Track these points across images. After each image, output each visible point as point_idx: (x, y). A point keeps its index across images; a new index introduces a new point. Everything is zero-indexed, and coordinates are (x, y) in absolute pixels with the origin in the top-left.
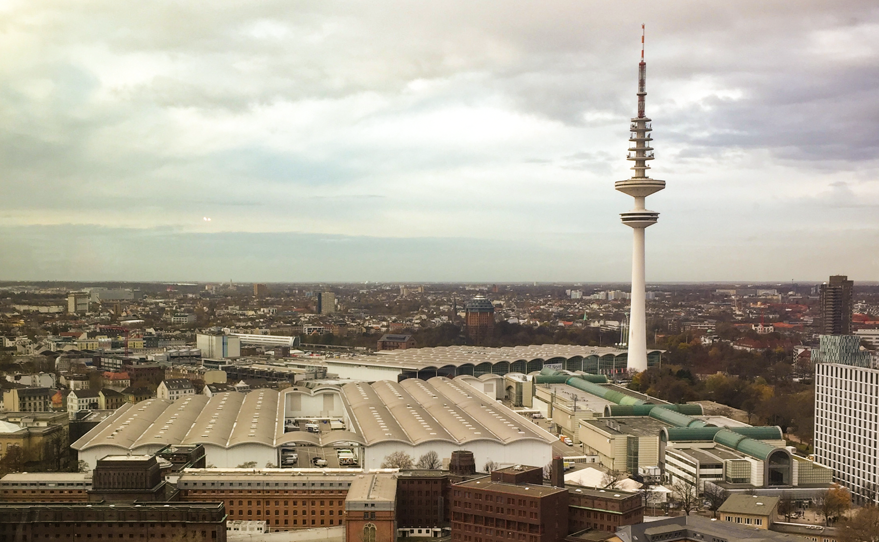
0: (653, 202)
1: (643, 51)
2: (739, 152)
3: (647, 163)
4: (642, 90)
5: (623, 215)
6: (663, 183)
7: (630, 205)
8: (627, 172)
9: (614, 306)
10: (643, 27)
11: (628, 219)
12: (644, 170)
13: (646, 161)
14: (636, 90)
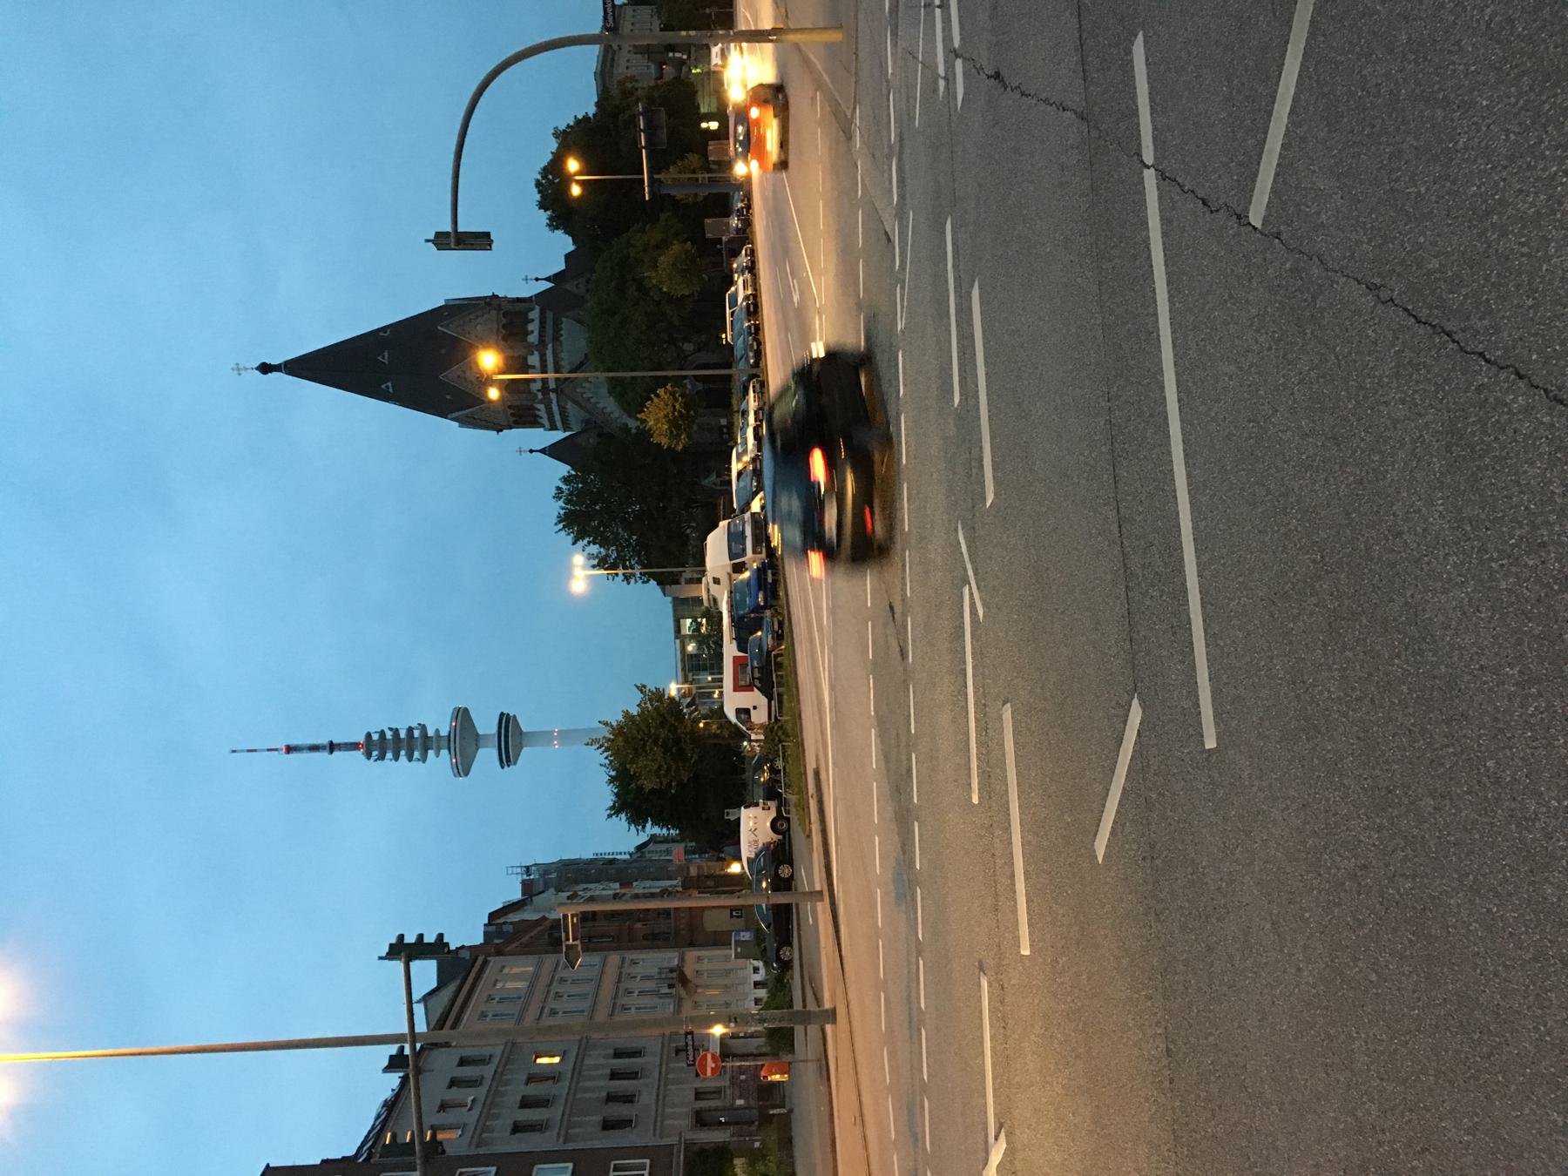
0: (486, 725)
7: (487, 756)
8: (441, 761)
10: (234, 751)
11: (506, 758)
14: (324, 755)
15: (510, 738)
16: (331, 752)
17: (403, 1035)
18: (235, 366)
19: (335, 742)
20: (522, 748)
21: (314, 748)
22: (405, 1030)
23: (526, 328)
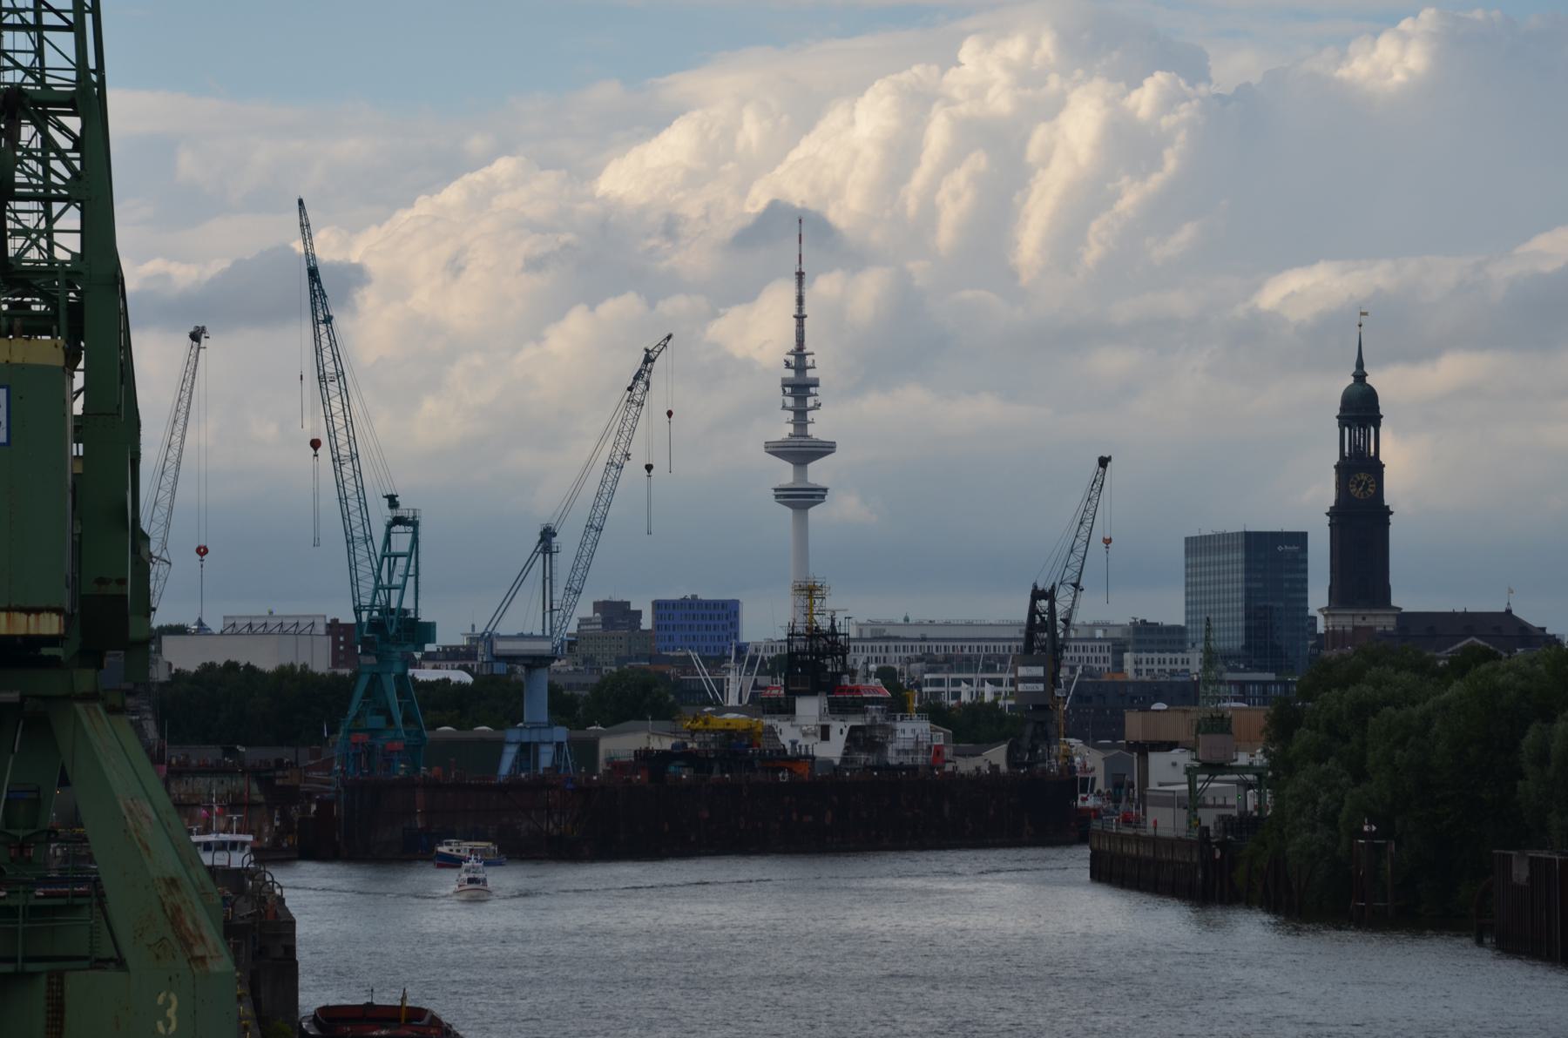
0: (817, 472)
1: (800, 235)
2: (830, 624)
3: (810, 415)
4: (800, 310)
5: (776, 490)
6: (833, 445)
8: (783, 429)
9: (759, 986)
10: (800, 221)
12: (806, 425)
13: (809, 413)
14: (795, 312)
15: (802, 498)
16: (795, 317)
17: (1153, 805)
18: (630, 457)
19: (805, 319)
20: (791, 508)
21: (800, 300)
22: (1172, 826)
23: (81, 442)
